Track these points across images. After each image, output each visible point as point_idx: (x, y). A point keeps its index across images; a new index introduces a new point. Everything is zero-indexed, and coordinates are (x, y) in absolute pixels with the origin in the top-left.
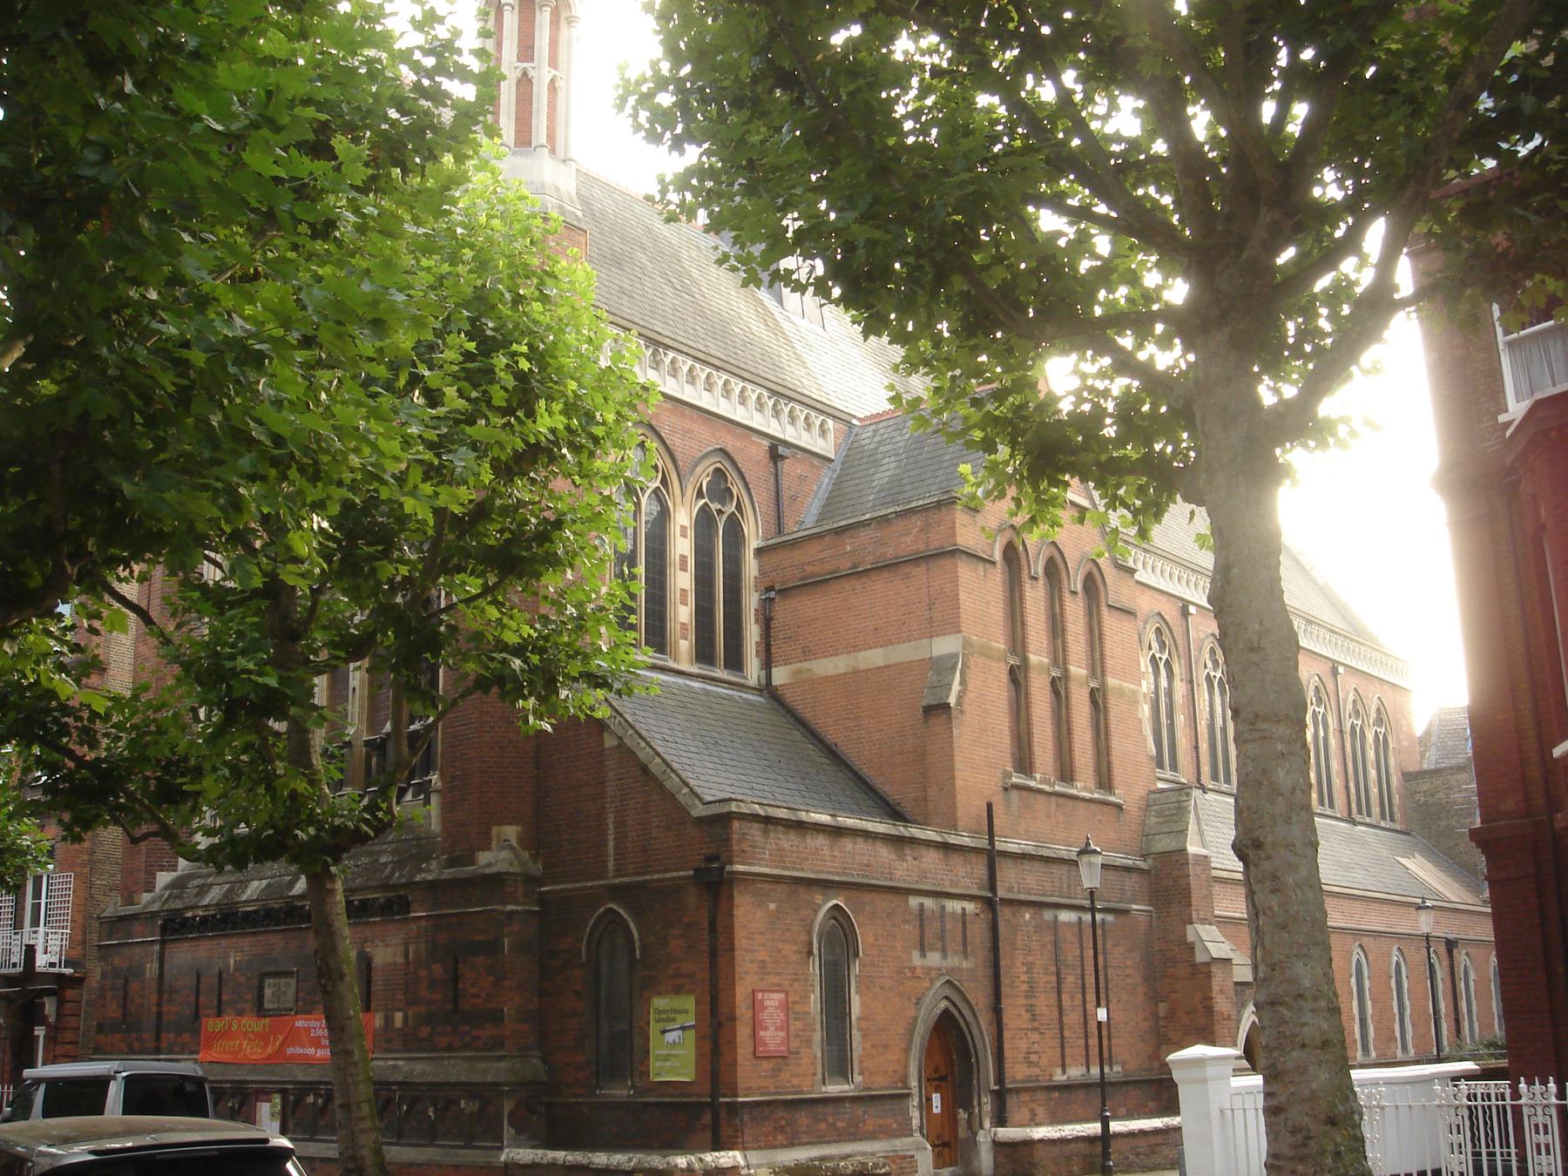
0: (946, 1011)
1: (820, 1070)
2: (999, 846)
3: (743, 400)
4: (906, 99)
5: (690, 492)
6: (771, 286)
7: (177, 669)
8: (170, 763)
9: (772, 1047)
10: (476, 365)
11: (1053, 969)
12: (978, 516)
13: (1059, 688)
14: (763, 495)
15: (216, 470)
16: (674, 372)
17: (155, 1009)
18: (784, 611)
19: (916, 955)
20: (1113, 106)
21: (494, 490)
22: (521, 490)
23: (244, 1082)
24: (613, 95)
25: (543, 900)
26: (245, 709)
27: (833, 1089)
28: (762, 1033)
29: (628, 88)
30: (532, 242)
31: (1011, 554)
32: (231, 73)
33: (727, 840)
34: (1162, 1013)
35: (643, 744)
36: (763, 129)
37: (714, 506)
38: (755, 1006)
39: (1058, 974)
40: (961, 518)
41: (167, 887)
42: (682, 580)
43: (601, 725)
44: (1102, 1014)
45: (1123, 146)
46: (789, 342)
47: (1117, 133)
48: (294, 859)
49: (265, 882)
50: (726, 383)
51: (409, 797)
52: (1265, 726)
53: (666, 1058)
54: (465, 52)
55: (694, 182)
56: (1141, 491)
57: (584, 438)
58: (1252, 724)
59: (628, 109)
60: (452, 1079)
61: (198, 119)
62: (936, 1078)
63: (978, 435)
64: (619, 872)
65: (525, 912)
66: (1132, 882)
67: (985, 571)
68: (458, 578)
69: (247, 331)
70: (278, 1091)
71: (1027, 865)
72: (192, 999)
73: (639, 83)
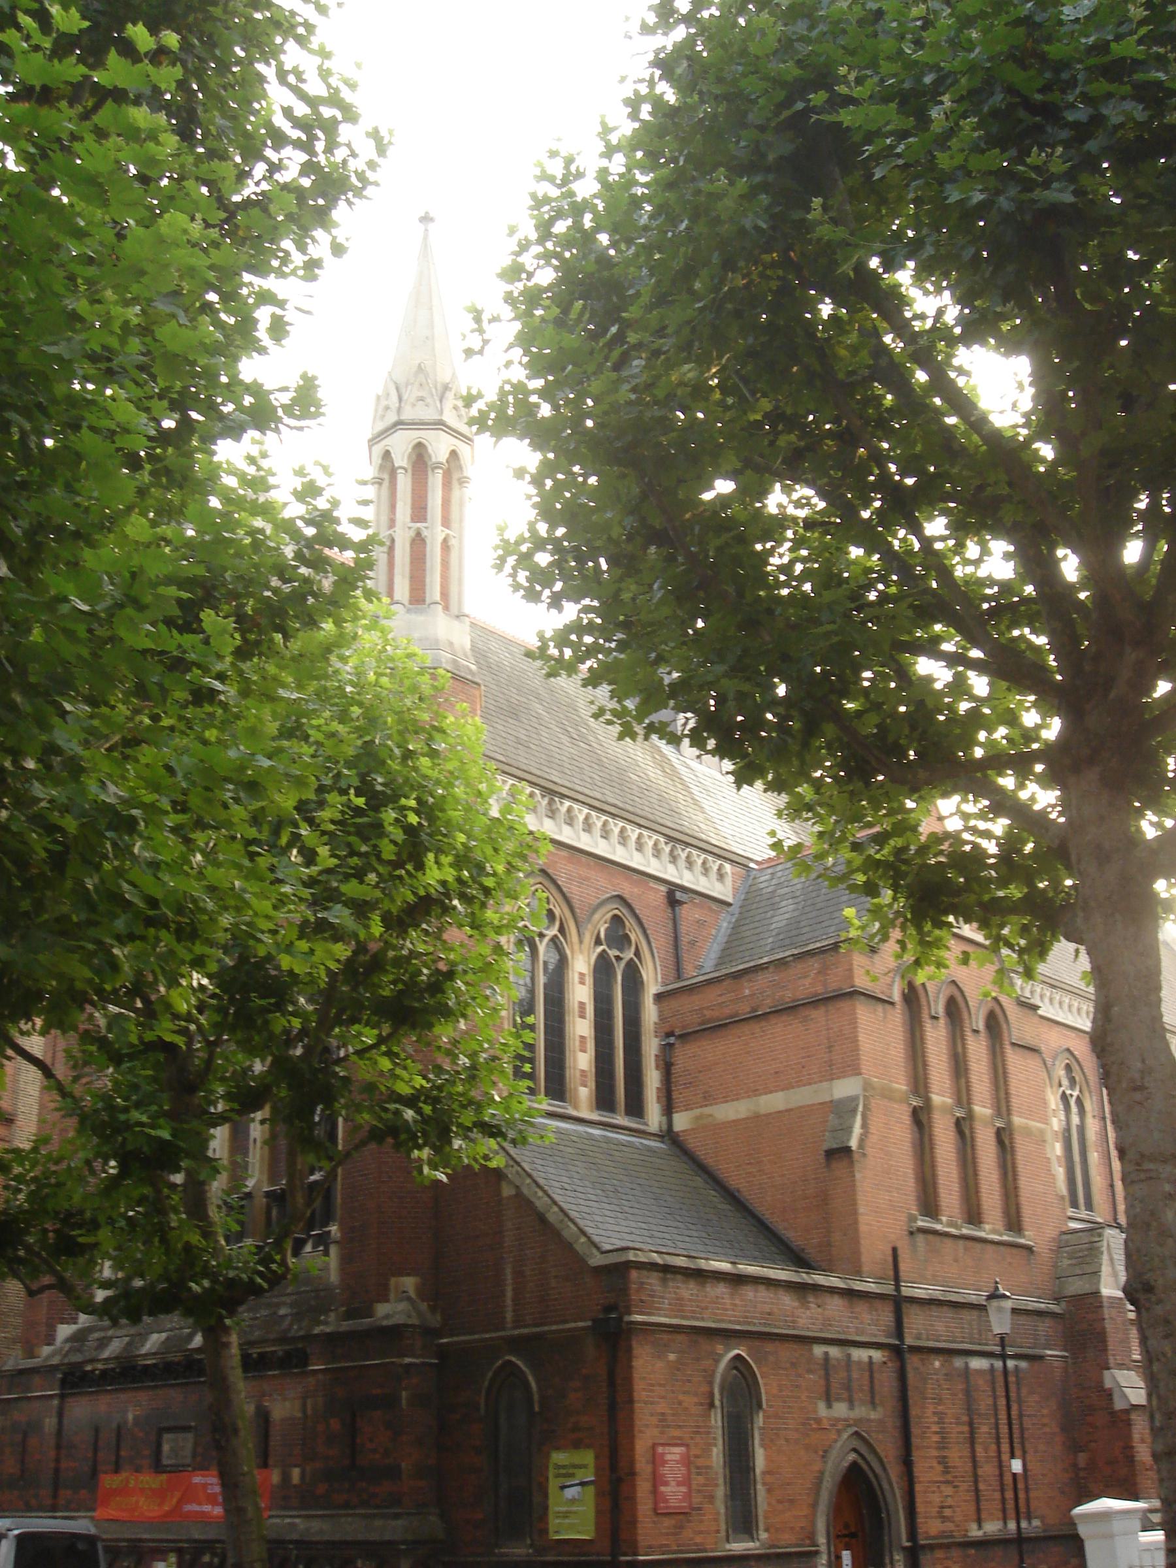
0: (854, 1464)
1: (723, 1527)
2: (906, 1291)
3: (640, 846)
4: (781, 550)
5: (588, 939)
6: (646, 738)
7: (72, 1122)
8: (69, 1215)
9: (673, 1503)
10: (365, 820)
11: (965, 1418)
12: (876, 957)
13: (963, 1129)
14: (661, 941)
15: (92, 932)
16: (570, 820)
17: (52, 1465)
18: (683, 1056)
19: (821, 1406)
20: (985, 551)
21: (386, 942)
22: (415, 942)
23: (140, 1540)
24: (492, 556)
25: (443, 1353)
26: (147, 1162)
27: (738, 1547)
28: (663, 1489)
29: (508, 548)
30: (421, 699)
31: (912, 997)
32: (100, 559)
33: (624, 1291)
34: (1082, 1464)
35: (540, 1193)
36: (633, 587)
37: (613, 953)
38: (656, 1460)
39: (971, 1424)
40: (859, 960)
41: (67, 1340)
42: (581, 1028)
43: (498, 1174)
44: (1017, 1466)
45: (996, 589)
46: (687, 788)
47: (989, 577)
48: (188, 1312)
49: (164, 1335)
50: (623, 830)
51: (308, 1248)
52: (1151, 1166)
53: (566, 1515)
54: (344, 520)
55: (573, 637)
56: (1024, 930)
57: (475, 888)
58: (1138, 1164)
59: (508, 569)
60: (349, 1538)
61: (66, 600)
62: (843, 1536)
63: (860, 878)
64: (518, 1323)
65: (423, 1364)
66: (1044, 1327)
67: (885, 1012)
68: (355, 1029)
69: (120, 797)
70: (172, 1550)
71: (935, 1311)
72: (90, 1455)
73: (518, 543)
